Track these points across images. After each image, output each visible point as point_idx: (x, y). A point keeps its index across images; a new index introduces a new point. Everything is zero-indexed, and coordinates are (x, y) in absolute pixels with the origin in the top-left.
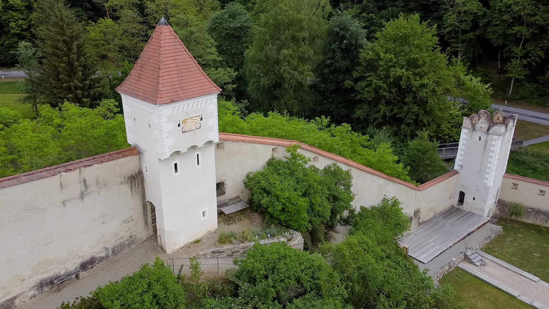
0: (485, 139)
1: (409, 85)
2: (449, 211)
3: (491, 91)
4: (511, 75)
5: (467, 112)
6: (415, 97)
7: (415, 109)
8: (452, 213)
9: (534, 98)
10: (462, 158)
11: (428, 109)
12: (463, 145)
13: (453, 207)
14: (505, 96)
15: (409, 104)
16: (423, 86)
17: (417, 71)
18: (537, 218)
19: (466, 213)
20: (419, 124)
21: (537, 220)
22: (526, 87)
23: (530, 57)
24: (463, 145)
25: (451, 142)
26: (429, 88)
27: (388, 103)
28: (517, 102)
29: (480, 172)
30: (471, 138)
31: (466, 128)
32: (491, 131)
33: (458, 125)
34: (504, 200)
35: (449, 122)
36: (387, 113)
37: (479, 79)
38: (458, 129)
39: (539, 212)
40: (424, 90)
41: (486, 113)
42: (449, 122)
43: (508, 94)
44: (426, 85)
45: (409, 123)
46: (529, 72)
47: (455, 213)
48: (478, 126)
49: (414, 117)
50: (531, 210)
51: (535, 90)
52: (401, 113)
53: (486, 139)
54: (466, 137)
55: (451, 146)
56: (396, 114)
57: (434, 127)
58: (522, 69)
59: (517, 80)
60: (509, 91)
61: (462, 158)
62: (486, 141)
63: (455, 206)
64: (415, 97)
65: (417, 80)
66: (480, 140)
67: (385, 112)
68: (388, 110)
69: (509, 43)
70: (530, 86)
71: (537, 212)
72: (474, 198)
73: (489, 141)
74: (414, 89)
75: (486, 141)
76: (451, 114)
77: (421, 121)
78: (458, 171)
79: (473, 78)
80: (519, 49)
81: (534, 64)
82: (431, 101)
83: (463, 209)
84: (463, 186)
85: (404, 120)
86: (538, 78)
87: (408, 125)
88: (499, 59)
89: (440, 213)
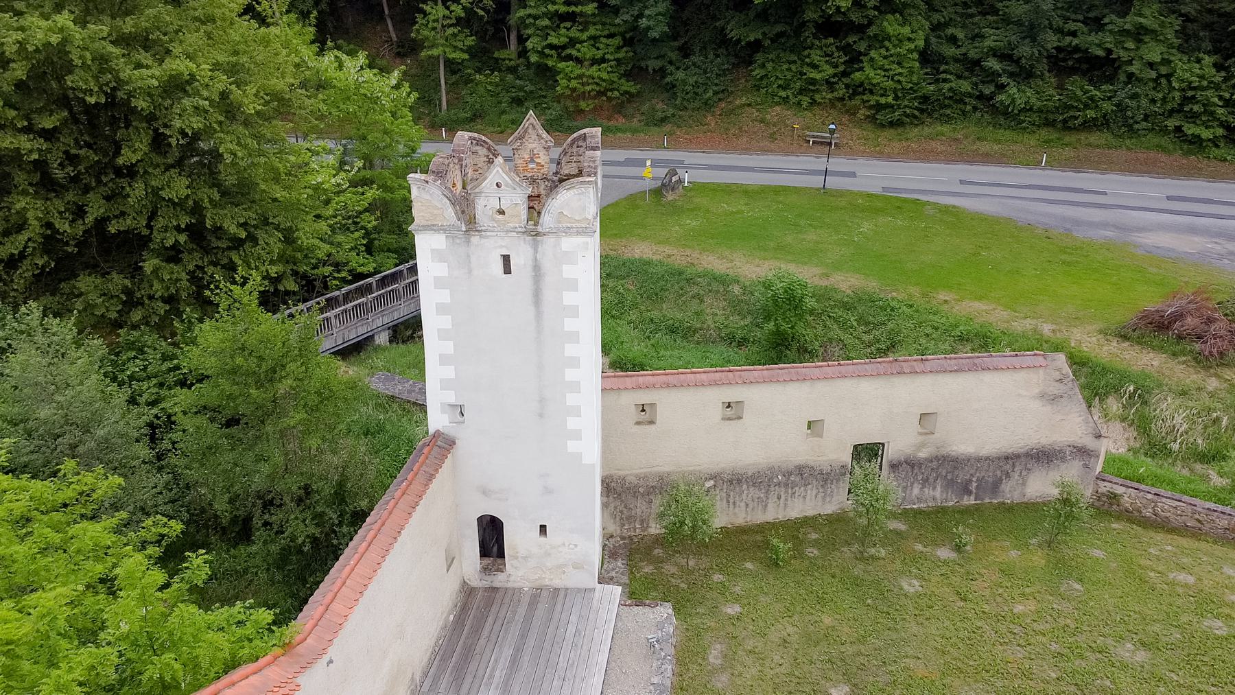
0: (530, 263)
1: (114, 89)
2: (459, 622)
3: (409, 94)
4: (435, 52)
5: (363, 173)
6: (159, 142)
7: (178, 187)
8: (477, 630)
9: (504, 112)
10: (449, 372)
11: (230, 180)
13: (468, 592)
14: (436, 116)
15: (146, 172)
16: (177, 86)
17: (128, 25)
18: (734, 503)
19: (526, 600)
20: (215, 243)
21: (737, 510)
22: (477, 85)
25: (345, 281)
26: (205, 93)
27: (47, 185)
28: (468, 127)
29: (541, 415)
30: (470, 271)
32: (547, 220)
33: (350, 221)
34: (621, 473)
35: (318, 217)
36: (63, 226)
37: (362, 58)
38: (352, 232)
39: (739, 481)
40: (186, 102)
41: (479, 143)
42: (318, 217)
44: (189, 83)
45: (175, 247)
46: (473, 38)
47: (490, 620)
48: (484, 205)
49: (185, 220)
50: (712, 482)
51: (500, 88)
52: (123, 214)
54: (441, 270)
55: (347, 298)
56: (101, 222)
57: (272, 242)
58: (456, 31)
59: (452, 67)
61: (449, 372)
62: (537, 271)
63: (475, 582)
64: (159, 142)
65: (145, 62)
66: (507, 269)
67: (49, 225)
68: (60, 213)
70: (486, 80)
71: (731, 482)
72: (543, 529)
73: (547, 265)
74: (141, 104)
75: (537, 271)
76: (317, 188)
77: (218, 230)
79: (344, 57)
82: (230, 146)
83: (510, 585)
84: (485, 492)
85: (149, 239)
86: (496, 55)
87: (173, 255)
88: (387, 12)
89: (430, 663)
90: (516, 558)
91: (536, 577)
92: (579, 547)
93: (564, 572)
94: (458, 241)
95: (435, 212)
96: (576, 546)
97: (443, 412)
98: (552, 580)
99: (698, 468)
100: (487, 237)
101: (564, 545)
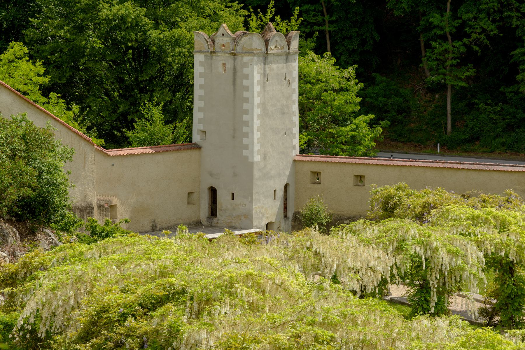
9: (497, 136)
12: (201, 87)
23: (469, 36)
24: (201, 87)
30: (211, 71)
31: (200, 52)
43: (446, 131)
53: (234, 66)
60: (446, 124)
62: (235, 70)
69: (425, 8)
73: (238, 68)
78: (200, 144)
80: (445, 18)
81: (476, 48)
84: (211, 175)
90: (221, 210)
91: (229, 221)
92: (247, 206)
93: (240, 219)
94: (208, 58)
95: (202, 45)
96: (245, 205)
97: (198, 134)
98: (235, 223)
99: (342, 213)
100: (218, 56)
101: (241, 204)
